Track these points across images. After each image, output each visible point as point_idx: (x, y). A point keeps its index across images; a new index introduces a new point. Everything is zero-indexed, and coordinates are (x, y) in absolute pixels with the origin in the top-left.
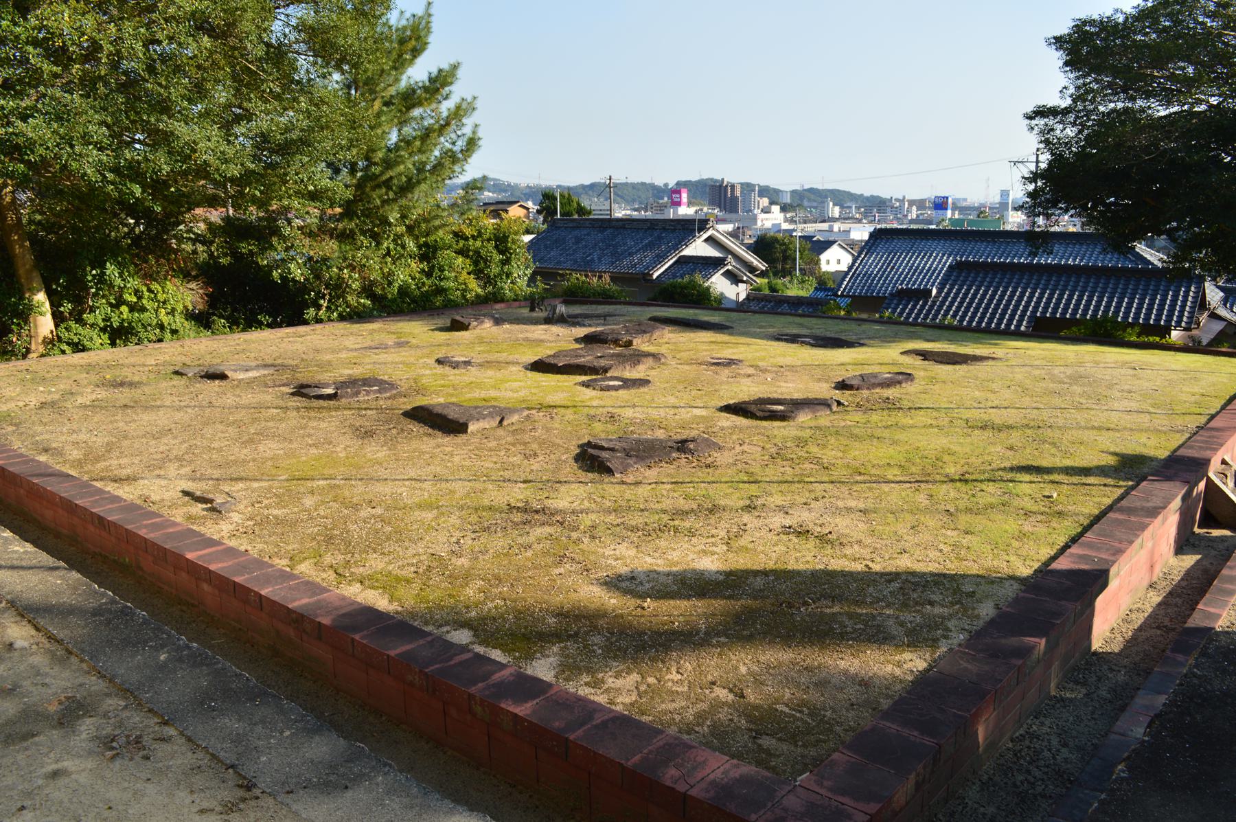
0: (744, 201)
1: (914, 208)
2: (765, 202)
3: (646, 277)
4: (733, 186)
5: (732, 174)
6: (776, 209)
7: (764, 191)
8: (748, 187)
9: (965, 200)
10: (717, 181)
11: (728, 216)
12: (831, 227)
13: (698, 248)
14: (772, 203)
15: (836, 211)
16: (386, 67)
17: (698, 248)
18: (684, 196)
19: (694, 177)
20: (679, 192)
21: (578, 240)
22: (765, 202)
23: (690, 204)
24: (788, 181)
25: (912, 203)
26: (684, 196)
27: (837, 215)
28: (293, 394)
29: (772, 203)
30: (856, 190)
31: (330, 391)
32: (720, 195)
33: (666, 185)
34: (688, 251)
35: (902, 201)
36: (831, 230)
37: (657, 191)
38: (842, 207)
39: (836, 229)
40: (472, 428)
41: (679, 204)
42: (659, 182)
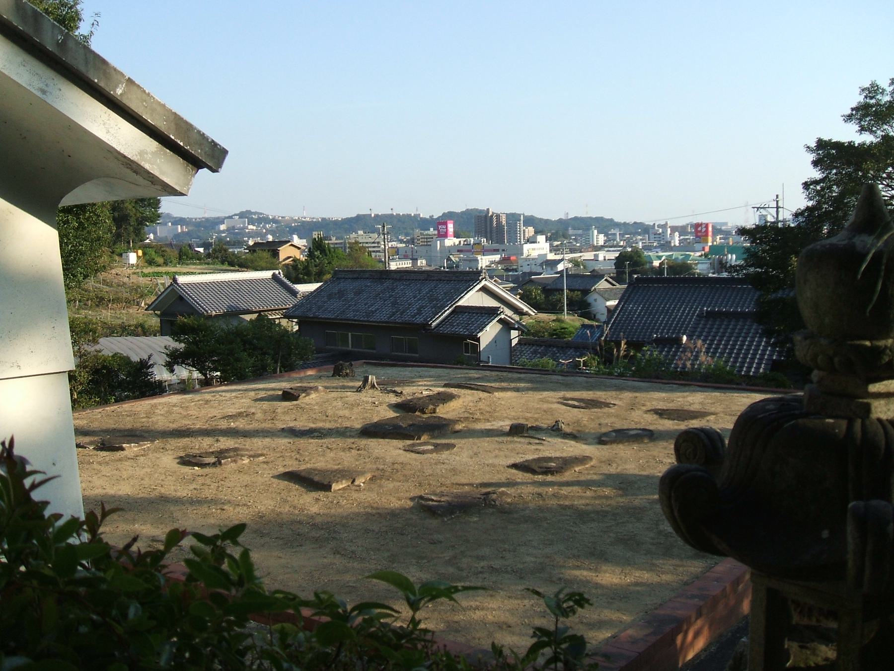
0: (509, 232)
1: (677, 234)
2: (530, 231)
3: (425, 326)
4: (498, 216)
5: (498, 204)
6: (541, 238)
7: (530, 221)
8: (513, 218)
9: (726, 224)
10: (481, 211)
11: (496, 246)
12: (596, 256)
13: (473, 298)
14: (537, 232)
15: (601, 239)
16: (285, 252)
17: (473, 298)
18: (451, 227)
19: (459, 208)
20: (446, 224)
21: (358, 293)
22: (530, 231)
23: (456, 235)
24: (552, 211)
25: (674, 229)
26: (451, 227)
27: (601, 243)
28: (643, 544)
29: (537, 232)
30: (618, 219)
31: (212, 460)
32: (485, 227)
33: (431, 217)
34: (462, 303)
35: (664, 227)
36: (596, 259)
37: (425, 223)
38: (606, 235)
39: (601, 258)
40: (335, 487)
41: (445, 235)
42: (424, 215)
